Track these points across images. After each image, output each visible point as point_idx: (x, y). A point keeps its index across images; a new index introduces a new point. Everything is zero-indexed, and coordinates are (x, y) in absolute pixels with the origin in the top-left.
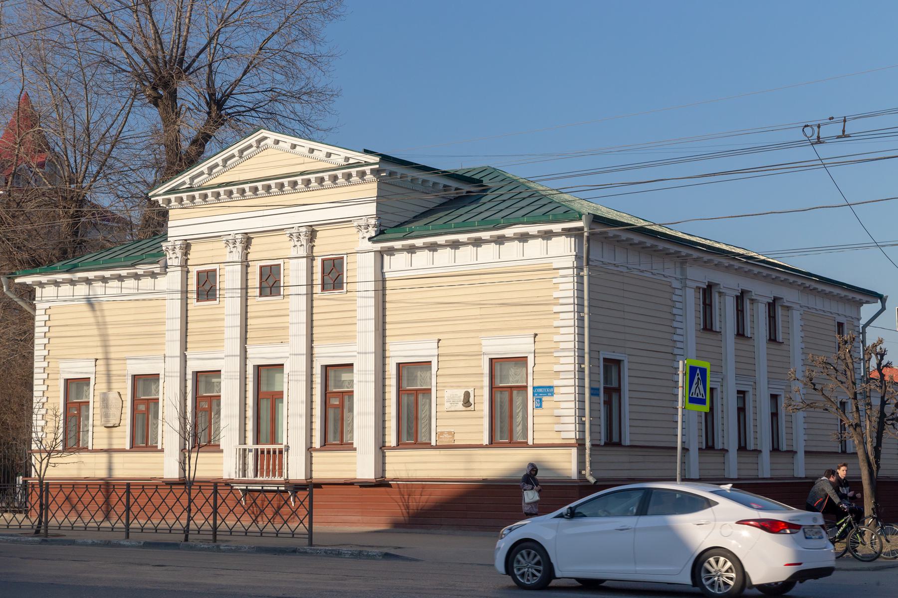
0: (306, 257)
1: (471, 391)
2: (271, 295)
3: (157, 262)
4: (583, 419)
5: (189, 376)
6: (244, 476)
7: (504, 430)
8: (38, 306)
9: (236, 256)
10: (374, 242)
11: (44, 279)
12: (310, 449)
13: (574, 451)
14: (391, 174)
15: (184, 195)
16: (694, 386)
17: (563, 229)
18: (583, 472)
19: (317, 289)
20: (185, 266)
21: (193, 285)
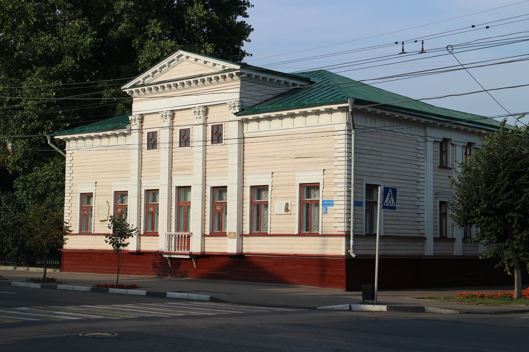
0: (203, 124)
1: (289, 203)
2: (185, 146)
3: (126, 128)
4: (350, 220)
5: (143, 193)
6: (169, 250)
7: (307, 227)
8: (67, 152)
9: (167, 123)
10: (237, 116)
11: (69, 137)
12: (204, 236)
13: (344, 239)
14: (249, 75)
15: (140, 89)
16: (387, 199)
17: (338, 108)
18: (349, 251)
19: (209, 143)
20: (141, 130)
21: (145, 141)
